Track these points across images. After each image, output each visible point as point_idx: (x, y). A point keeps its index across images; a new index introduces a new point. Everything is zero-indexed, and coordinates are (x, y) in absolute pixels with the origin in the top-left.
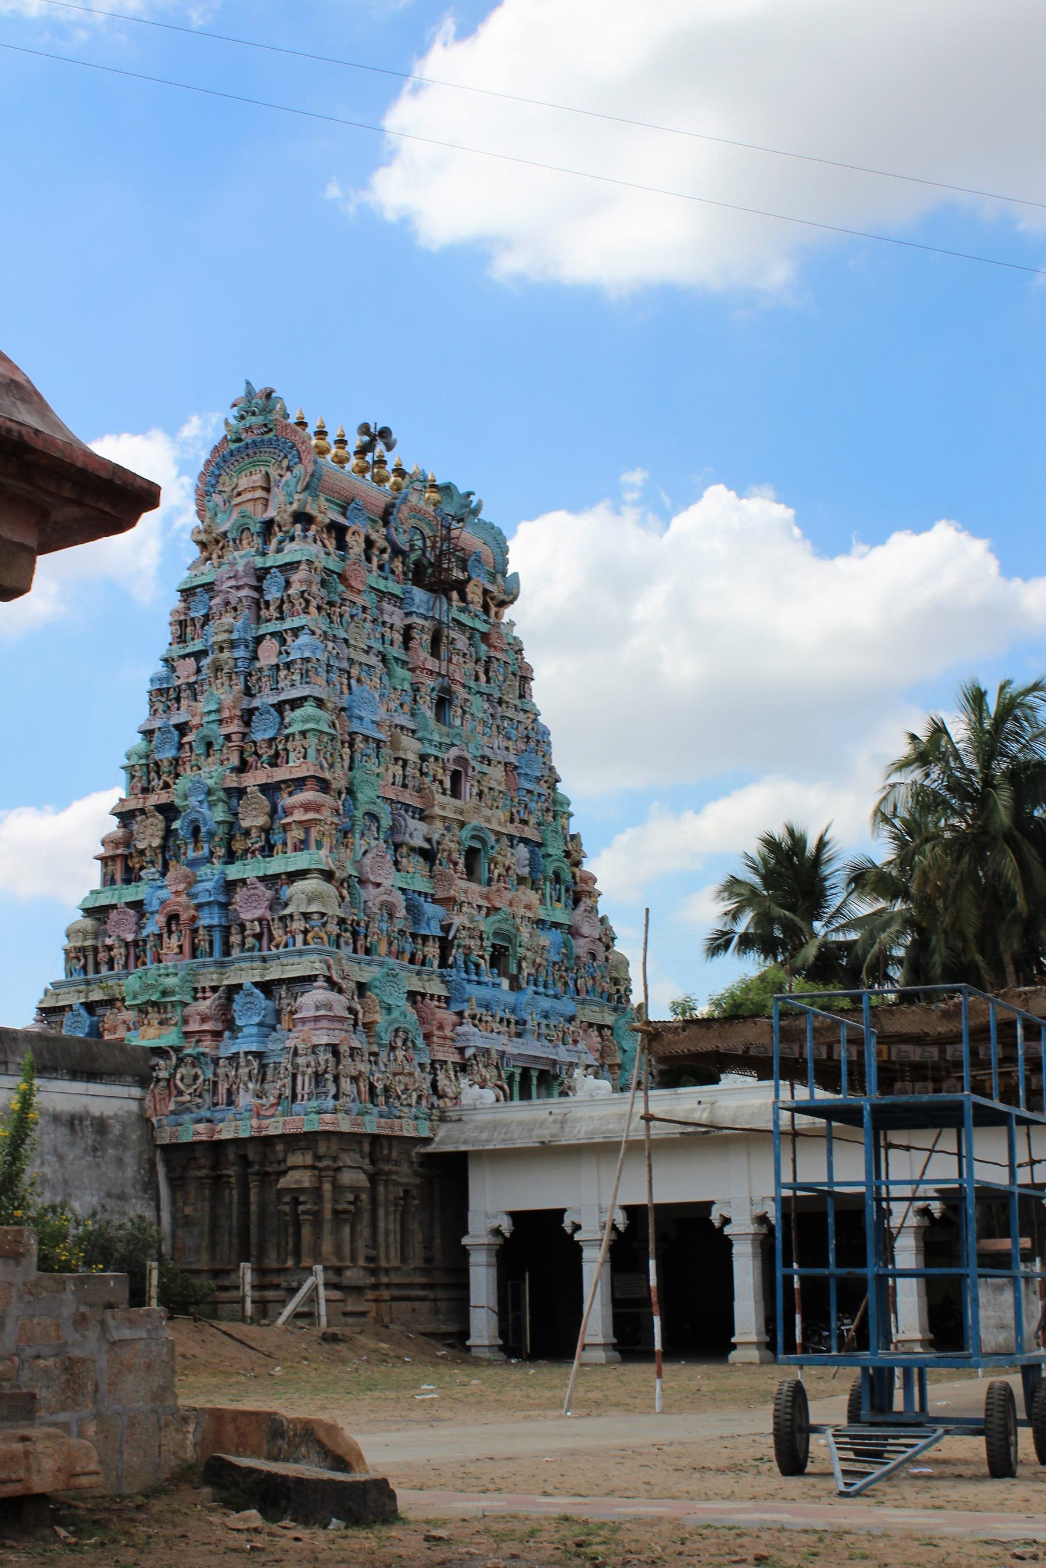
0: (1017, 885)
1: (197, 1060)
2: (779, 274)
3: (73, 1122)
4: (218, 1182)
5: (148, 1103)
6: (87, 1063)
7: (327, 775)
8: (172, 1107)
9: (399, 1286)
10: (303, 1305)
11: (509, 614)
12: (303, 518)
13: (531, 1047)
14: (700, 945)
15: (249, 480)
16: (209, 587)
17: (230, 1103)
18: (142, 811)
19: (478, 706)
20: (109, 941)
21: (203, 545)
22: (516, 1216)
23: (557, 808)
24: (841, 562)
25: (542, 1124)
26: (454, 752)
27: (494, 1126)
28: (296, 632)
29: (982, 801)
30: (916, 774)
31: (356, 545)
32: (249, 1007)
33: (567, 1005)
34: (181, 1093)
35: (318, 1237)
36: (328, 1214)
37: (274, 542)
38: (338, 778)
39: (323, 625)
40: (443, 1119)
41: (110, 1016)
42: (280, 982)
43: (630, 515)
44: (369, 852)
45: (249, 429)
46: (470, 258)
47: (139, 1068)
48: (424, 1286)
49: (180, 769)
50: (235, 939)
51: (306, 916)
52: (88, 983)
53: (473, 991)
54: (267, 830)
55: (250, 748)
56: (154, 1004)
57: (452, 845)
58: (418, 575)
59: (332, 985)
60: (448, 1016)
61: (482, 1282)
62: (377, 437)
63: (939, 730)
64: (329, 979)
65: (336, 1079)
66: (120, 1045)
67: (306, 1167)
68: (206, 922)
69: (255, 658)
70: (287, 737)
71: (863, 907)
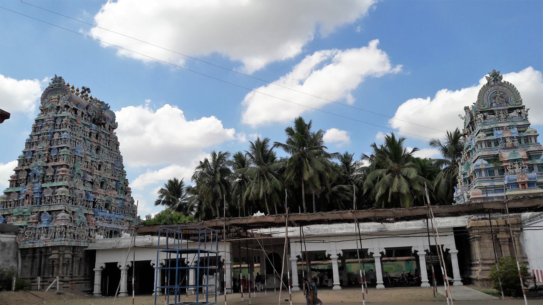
0: (220, 193)
1: (31, 229)
2: (181, 62)
4: (34, 257)
5: (17, 239)
10: (251, 98)
11: (115, 131)
13: (113, 226)
14: (154, 203)
16: (43, 120)
17: (39, 239)
18: (22, 170)
19: (106, 150)
21: (42, 110)
22: (106, 264)
23: (123, 173)
24: (191, 122)
25: (114, 243)
26: (100, 160)
27: (103, 244)
28: (63, 132)
29: (214, 175)
30: (201, 170)
31: (79, 114)
32: (45, 217)
33: (122, 217)
34: (26, 236)
36: (61, 264)
38: (71, 165)
39: (70, 130)
40: (91, 242)
41: (9, 218)
42: (53, 211)
46: (112, 50)
48: (83, 280)
50: (43, 201)
51: (61, 196)
53: (100, 214)
54: (53, 176)
56: (21, 215)
58: (94, 121)
60: (94, 219)
62: (86, 90)
63: (206, 161)
64: (65, 211)
65: (65, 233)
66: (11, 225)
71: (189, 196)
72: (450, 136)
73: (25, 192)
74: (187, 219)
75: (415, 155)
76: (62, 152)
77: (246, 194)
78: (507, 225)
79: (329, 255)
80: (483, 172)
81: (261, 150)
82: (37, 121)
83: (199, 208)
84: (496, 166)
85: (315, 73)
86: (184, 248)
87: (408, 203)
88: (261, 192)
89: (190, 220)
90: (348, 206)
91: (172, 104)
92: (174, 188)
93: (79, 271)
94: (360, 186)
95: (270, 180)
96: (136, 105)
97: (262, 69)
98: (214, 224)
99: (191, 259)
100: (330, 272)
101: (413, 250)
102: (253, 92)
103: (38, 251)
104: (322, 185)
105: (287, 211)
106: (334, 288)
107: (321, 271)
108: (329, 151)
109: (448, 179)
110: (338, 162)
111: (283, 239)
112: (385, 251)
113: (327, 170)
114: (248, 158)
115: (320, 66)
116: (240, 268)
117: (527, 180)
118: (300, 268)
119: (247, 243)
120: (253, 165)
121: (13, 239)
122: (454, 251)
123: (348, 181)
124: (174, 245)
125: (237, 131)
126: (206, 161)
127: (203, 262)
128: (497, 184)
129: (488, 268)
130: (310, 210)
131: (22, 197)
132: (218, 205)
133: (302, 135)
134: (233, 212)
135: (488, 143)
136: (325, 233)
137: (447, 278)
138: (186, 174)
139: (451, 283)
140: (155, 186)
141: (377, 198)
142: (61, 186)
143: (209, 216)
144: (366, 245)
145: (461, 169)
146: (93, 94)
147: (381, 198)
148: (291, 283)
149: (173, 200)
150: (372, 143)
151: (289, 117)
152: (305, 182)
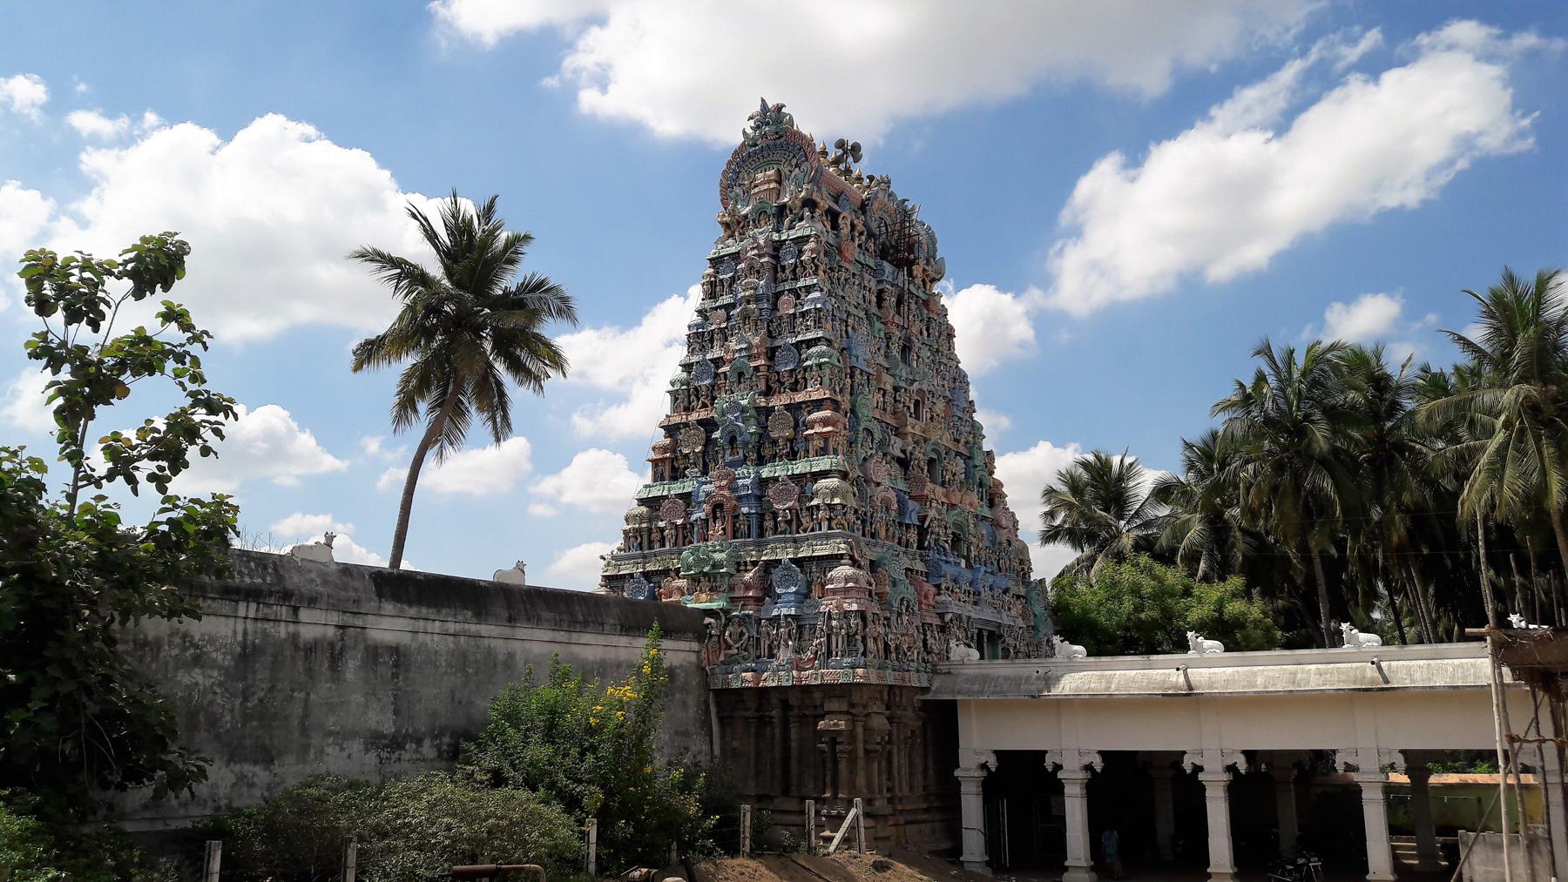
4: (763, 722)
5: (704, 655)
7: (839, 398)
8: (722, 658)
9: (909, 811)
12: (809, 203)
13: (988, 614)
15: (764, 176)
16: (736, 257)
17: (772, 656)
18: (686, 425)
19: (925, 353)
20: (661, 524)
21: (727, 226)
25: (1028, 679)
28: (808, 289)
32: (786, 582)
34: (729, 647)
35: (853, 773)
37: (787, 221)
40: (935, 672)
42: (811, 559)
45: (764, 136)
47: (677, 623)
48: (927, 810)
49: (716, 393)
50: (769, 524)
51: (831, 507)
52: (644, 557)
54: (791, 441)
55: (774, 377)
57: (920, 456)
58: (883, 254)
59: (855, 563)
64: (852, 558)
65: (864, 639)
66: (678, 608)
67: (841, 713)
68: (745, 510)
69: (775, 308)
70: (805, 369)
73: (708, 494)
93: (911, 774)
103: (774, 701)
121: (693, 658)
142: (824, 474)
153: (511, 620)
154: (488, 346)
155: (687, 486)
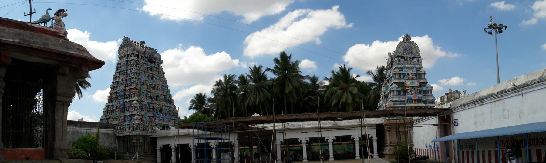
0: (230, 101)
1: (121, 125)
2: (201, 19)
3: (105, 134)
4: (124, 141)
6: (106, 126)
10: (250, 39)
11: (161, 65)
12: (133, 54)
13: (165, 123)
14: (188, 109)
19: (157, 78)
22: (163, 145)
23: (168, 91)
24: (209, 56)
27: (160, 133)
29: (226, 90)
30: (217, 87)
31: (140, 57)
32: (128, 118)
33: (170, 117)
38: (139, 88)
41: (109, 120)
43: (180, 50)
44: (143, 96)
46: (157, 17)
53: (157, 115)
58: (149, 61)
59: (138, 115)
60: (154, 119)
61: (159, 154)
62: (143, 43)
63: (220, 81)
71: (210, 104)
72: (378, 69)
74: (209, 119)
75: (358, 79)
76: (133, 80)
77: (247, 102)
78: (405, 123)
79: (301, 141)
80: (395, 92)
81: (256, 72)
82: (118, 64)
83: (217, 111)
84: (402, 89)
85: (294, 23)
86: (209, 136)
87: (351, 109)
88: (257, 101)
89: (212, 119)
90: (314, 110)
91: (196, 45)
92: (200, 100)
94: (322, 97)
95: (263, 93)
96: (172, 48)
97: (257, 21)
98: (227, 122)
99: (213, 143)
100: (301, 151)
101: (352, 137)
102: (251, 35)
104: (297, 96)
105: (274, 113)
106: (304, 161)
107: (295, 150)
108: (302, 74)
109: (375, 95)
110: (308, 81)
111: (271, 131)
112: (335, 138)
113: (301, 87)
114: (248, 78)
115: (298, 19)
116: (244, 149)
117: (417, 98)
118: (282, 149)
119: (248, 133)
120: (251, 83)
122: (375, 137)
123: (314, 94)
124: (202, 135)
125: (241, 60)
126: (220, 81)
127: (221, 145)
128: (402, 99)
129: (393, 148)
130: (289, 112)
131: (114, 108)
132: (229, 109)
133: (285, 64)
134: (239, 114)
135: (400, 75)
136: (299, 127)
137: (370, 154)
138: (208, 90)
139: (372, 157)
140: (188, 98)
141: (332, 105)
142: (134, 101)
143: (223, 117)
144: (324, 134)
145: (383, 89)
146: (147, 45)
147: (335, 105)
148: (277, 158)
149: (200, 106)
150: (332, 70)
151: (276, 51)
152: (286, 94)
153: (81, 127)
154: (77, 83)
155: (113, 103)
